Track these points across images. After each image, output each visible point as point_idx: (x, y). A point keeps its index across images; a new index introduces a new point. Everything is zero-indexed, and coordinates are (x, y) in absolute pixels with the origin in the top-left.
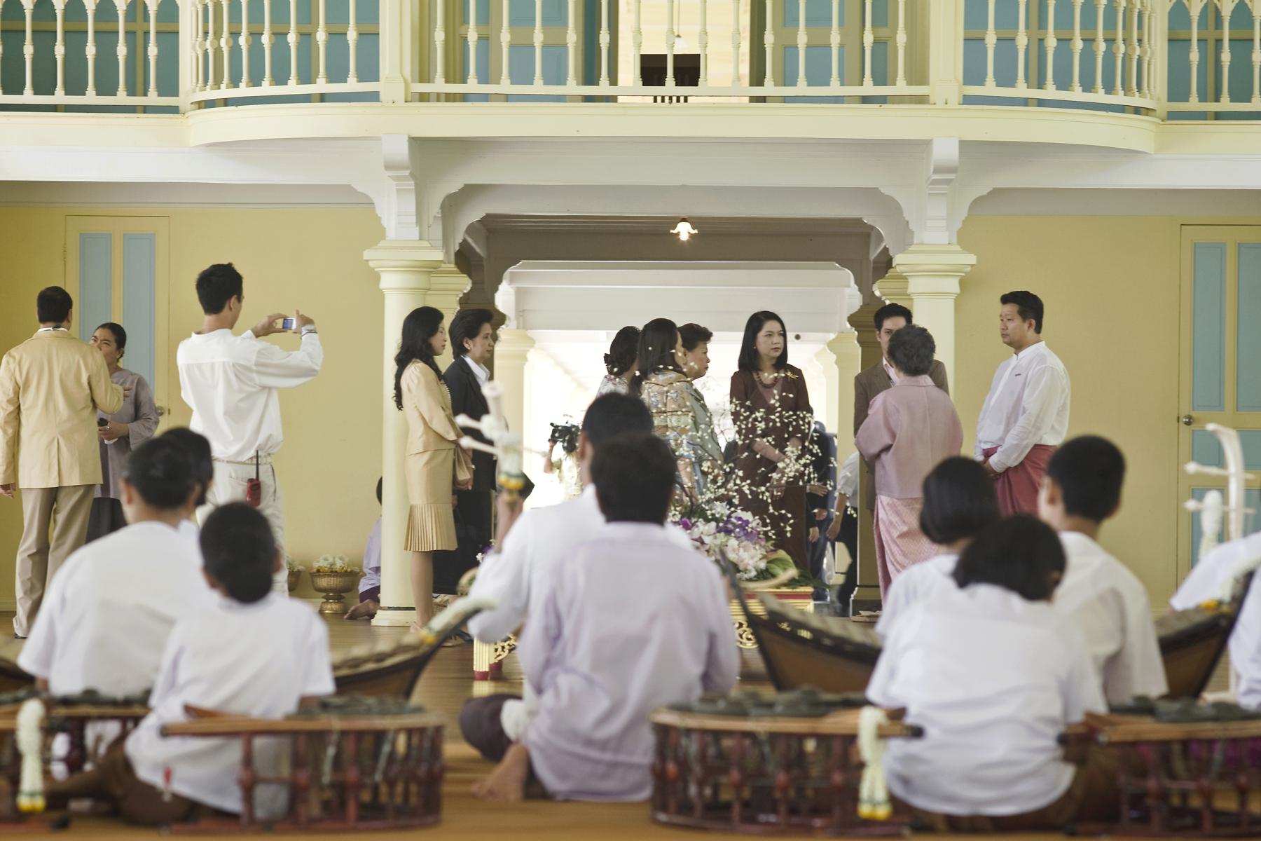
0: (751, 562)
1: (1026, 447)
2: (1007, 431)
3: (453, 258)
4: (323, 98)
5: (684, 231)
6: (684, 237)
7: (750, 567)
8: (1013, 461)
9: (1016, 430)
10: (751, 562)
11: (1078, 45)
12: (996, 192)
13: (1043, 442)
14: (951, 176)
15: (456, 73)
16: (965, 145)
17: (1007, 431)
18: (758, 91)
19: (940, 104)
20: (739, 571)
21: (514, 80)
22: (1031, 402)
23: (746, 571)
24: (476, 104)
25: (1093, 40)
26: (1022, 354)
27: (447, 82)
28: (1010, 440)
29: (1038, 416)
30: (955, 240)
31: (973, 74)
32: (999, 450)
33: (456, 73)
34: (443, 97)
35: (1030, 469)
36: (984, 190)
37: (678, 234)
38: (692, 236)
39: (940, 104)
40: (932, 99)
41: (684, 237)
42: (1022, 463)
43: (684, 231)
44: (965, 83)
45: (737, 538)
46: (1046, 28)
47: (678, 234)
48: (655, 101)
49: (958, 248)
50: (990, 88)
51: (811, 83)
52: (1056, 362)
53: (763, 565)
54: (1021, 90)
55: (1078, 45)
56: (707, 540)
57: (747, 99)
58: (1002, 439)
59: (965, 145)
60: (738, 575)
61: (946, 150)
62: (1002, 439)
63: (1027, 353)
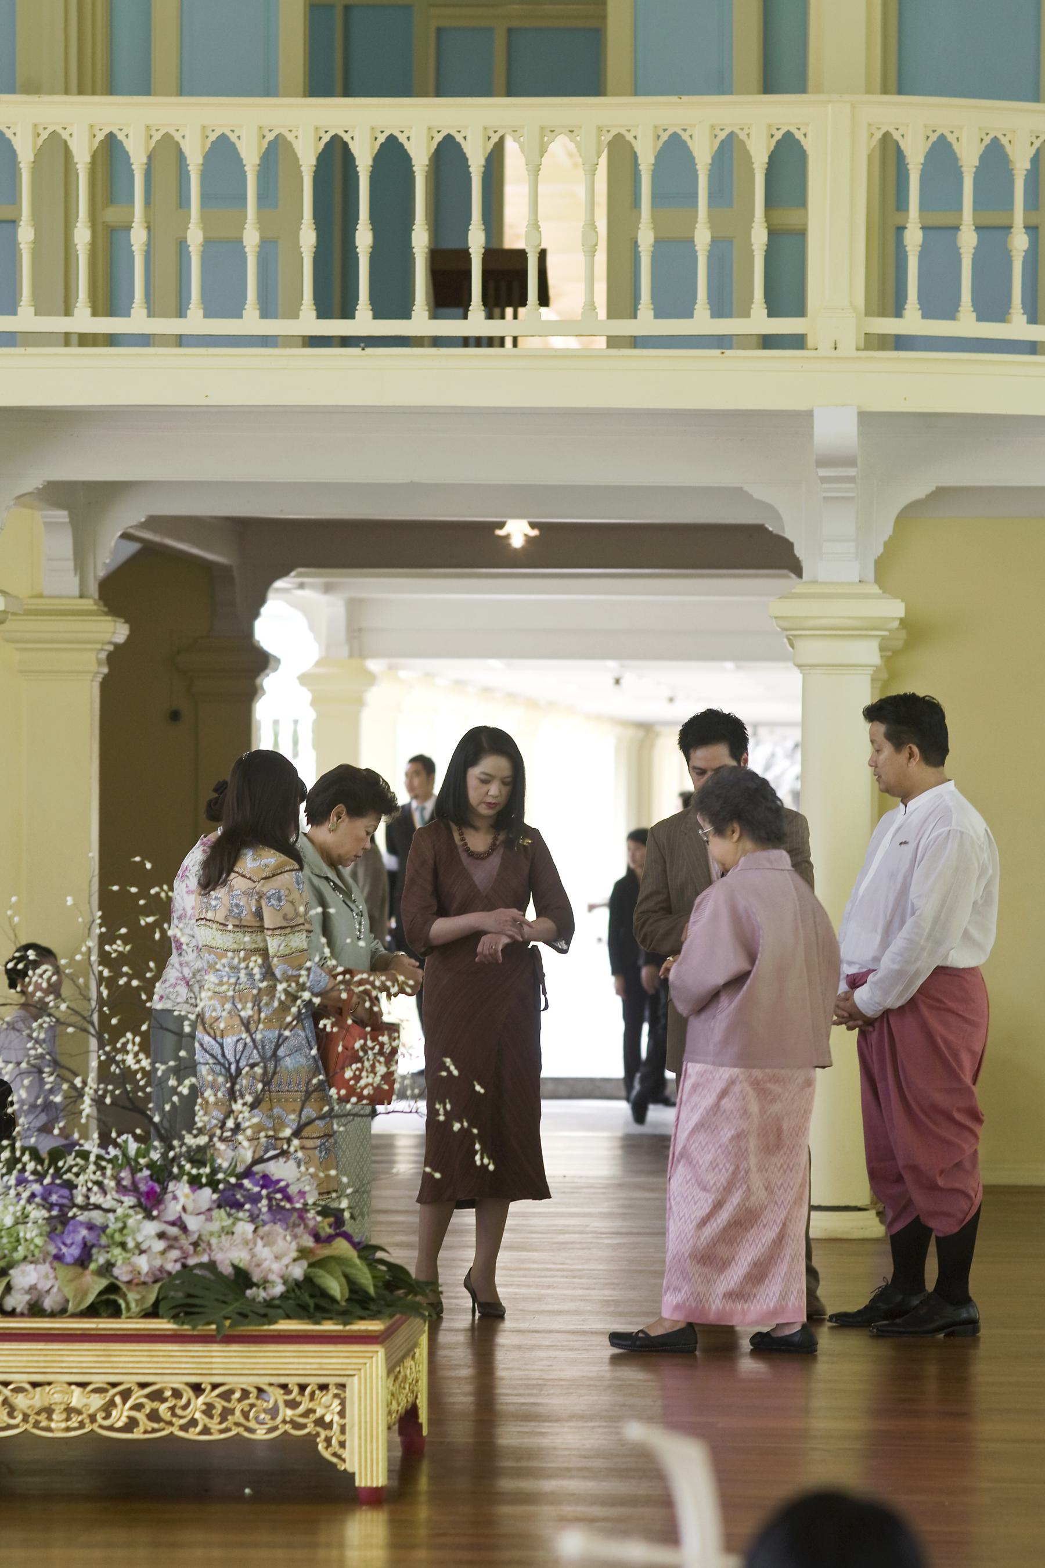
0: (276, 1267)
1: (917, 974)
2: (885, 944)
3: (93, 589)
4: (86, 340)
5: (517, 532)
6: (517, 542)
7: (272, 1277)
8: (894, 1001)
9: (898, 944)
10: (276, 1267)
11: (968, 239)
12: (941, 494)
13: (949, 963)
14: (851, 472)
15: (335, 300)
16: (867, 419)
17: (885, 944)
18: (626, 327)
19: (825, 349)
20: (251, 1285)
21: (323, 312)
22: (925, 899)
23: (265, 1283)
24: (31, 350)
25: (957, 228)
26: (912, 804)
27: (95, 314)
28: (887, 963)
29: (936, 920)
30: (871, 576)
31: (888, 297)
32: (871, 978)
33: (109, 299)
34: (75, 339)
35: (925, 1010)
36: (920, 490)
37: (507, 537)
38: (529, 540)
39: (825, 349)
40: (810, 342)
41: (517, 542)
42: (912, 1001)
43: (517, 532)
44: (868, 313)
45: (253, 1218)
46: (907, 210)
47: (507, 537)
48: (515, 340)
49: (876, 589)
50: (912, 322)
51: (379, 313)
52: (975, 823)
53: (298, 1272)
54: (967, 324)
55: (968, 239)
56: (193, 1223)
57: (601, 343)
58: (877, 959)
59: (867, 419)
60: (249, 1293)
61: (835, 429)
62: (877, 959)
63: (920, 803)
